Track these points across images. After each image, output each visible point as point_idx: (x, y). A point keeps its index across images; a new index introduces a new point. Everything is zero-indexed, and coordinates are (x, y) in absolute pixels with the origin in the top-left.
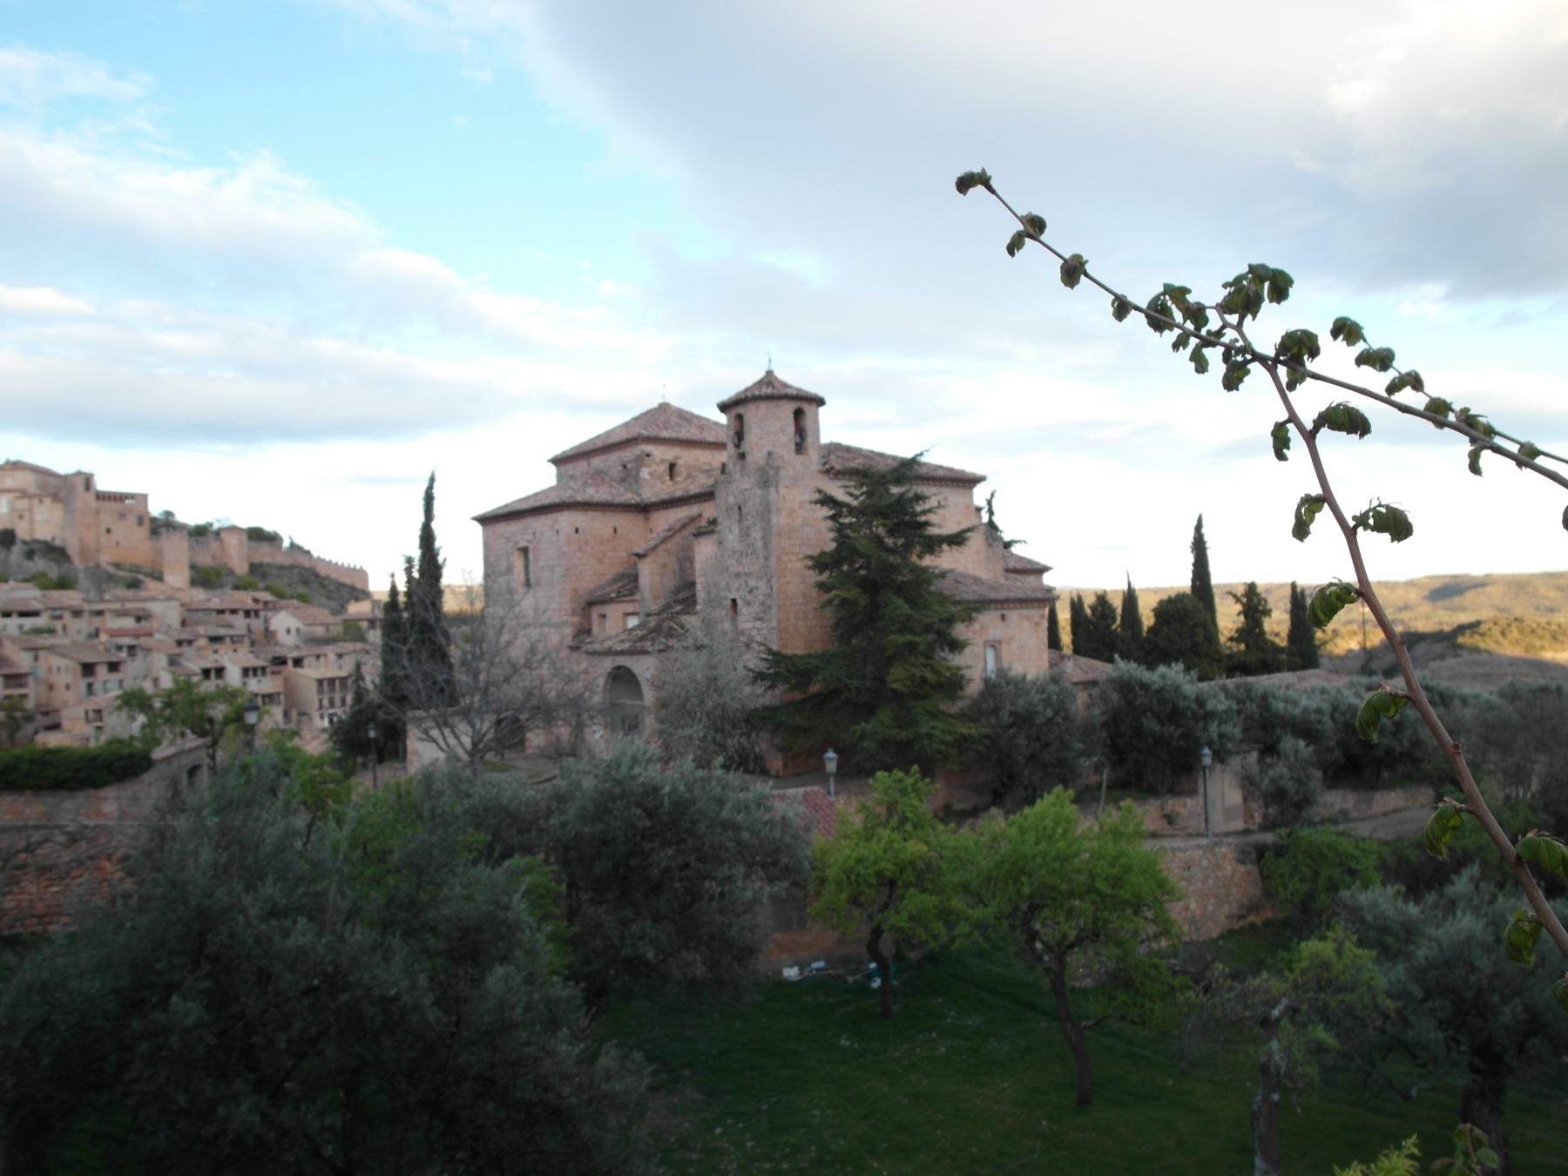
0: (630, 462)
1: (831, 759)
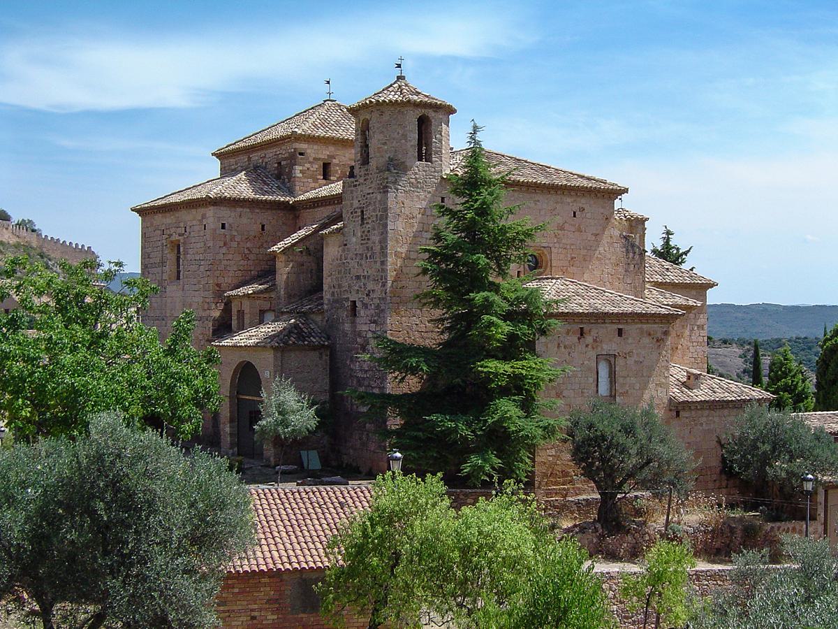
0: (285, 159)
1: (397, 459)
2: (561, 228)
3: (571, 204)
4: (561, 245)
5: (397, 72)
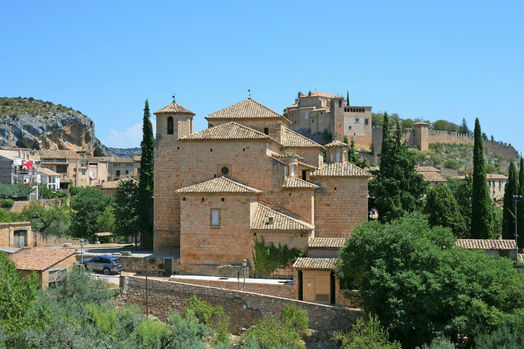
2: (237, 156)
3: (242, 145)
4: (237, 163)
5: (173, 99)
